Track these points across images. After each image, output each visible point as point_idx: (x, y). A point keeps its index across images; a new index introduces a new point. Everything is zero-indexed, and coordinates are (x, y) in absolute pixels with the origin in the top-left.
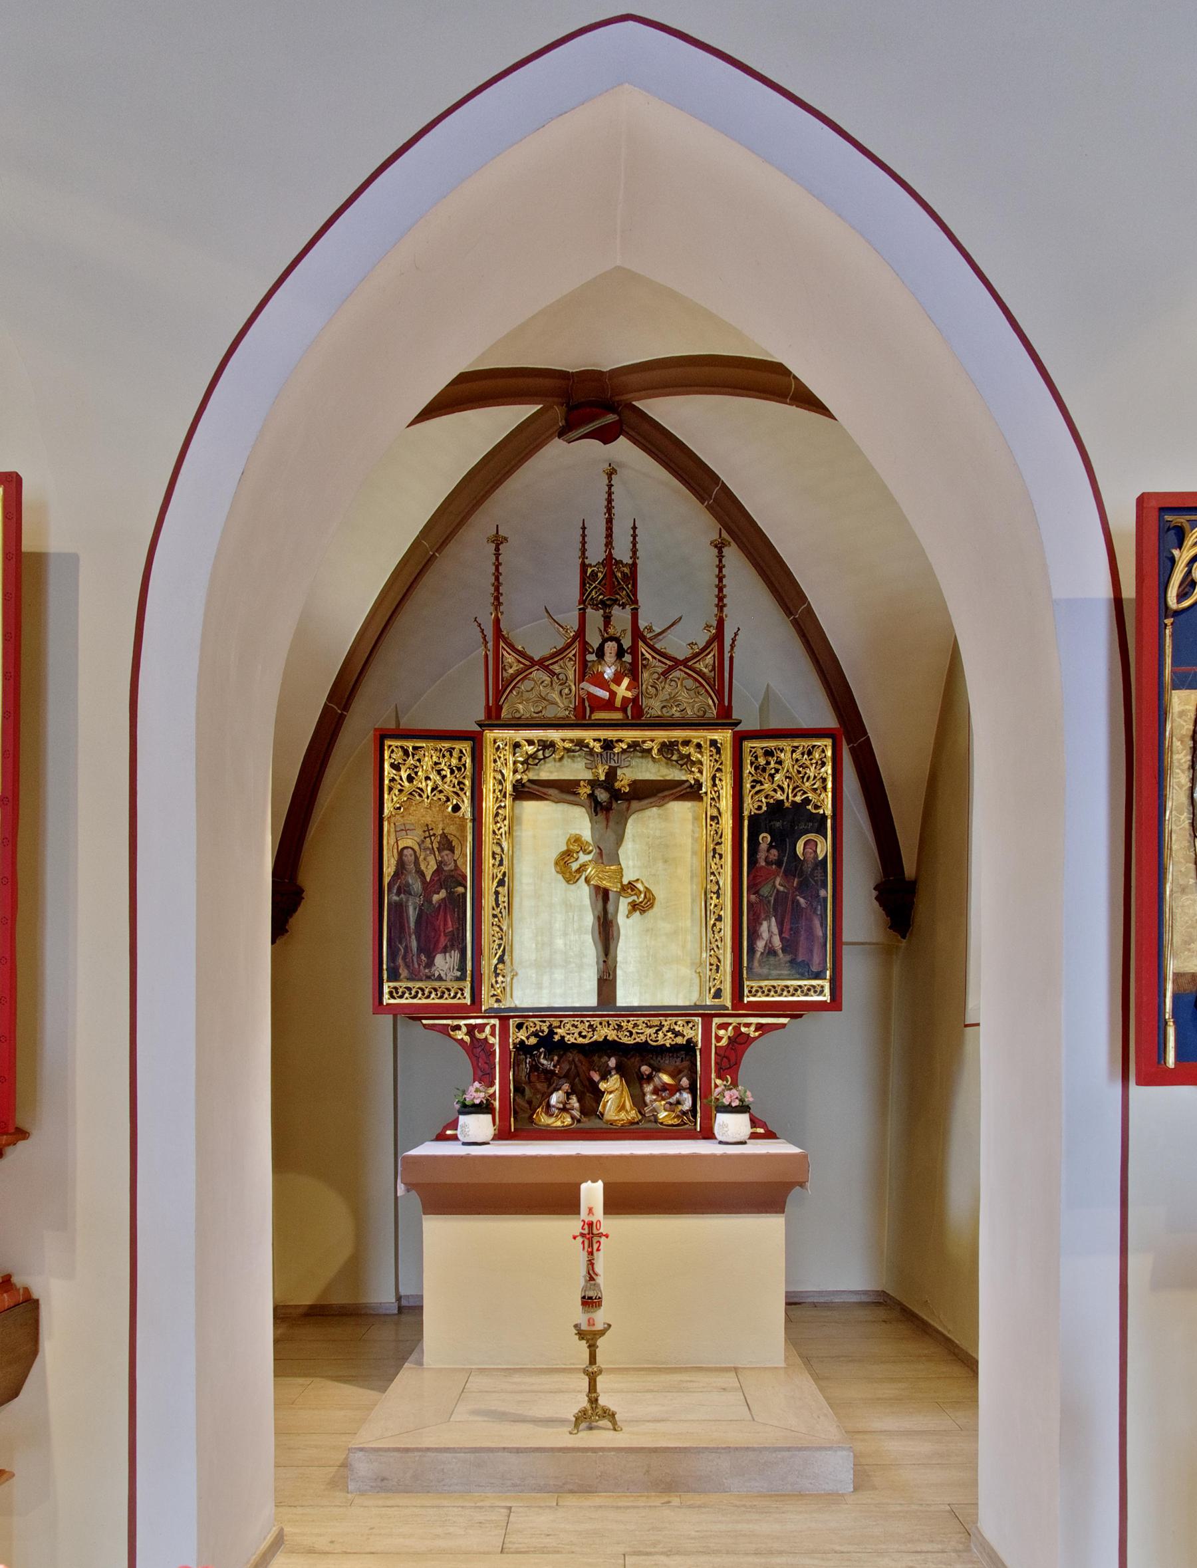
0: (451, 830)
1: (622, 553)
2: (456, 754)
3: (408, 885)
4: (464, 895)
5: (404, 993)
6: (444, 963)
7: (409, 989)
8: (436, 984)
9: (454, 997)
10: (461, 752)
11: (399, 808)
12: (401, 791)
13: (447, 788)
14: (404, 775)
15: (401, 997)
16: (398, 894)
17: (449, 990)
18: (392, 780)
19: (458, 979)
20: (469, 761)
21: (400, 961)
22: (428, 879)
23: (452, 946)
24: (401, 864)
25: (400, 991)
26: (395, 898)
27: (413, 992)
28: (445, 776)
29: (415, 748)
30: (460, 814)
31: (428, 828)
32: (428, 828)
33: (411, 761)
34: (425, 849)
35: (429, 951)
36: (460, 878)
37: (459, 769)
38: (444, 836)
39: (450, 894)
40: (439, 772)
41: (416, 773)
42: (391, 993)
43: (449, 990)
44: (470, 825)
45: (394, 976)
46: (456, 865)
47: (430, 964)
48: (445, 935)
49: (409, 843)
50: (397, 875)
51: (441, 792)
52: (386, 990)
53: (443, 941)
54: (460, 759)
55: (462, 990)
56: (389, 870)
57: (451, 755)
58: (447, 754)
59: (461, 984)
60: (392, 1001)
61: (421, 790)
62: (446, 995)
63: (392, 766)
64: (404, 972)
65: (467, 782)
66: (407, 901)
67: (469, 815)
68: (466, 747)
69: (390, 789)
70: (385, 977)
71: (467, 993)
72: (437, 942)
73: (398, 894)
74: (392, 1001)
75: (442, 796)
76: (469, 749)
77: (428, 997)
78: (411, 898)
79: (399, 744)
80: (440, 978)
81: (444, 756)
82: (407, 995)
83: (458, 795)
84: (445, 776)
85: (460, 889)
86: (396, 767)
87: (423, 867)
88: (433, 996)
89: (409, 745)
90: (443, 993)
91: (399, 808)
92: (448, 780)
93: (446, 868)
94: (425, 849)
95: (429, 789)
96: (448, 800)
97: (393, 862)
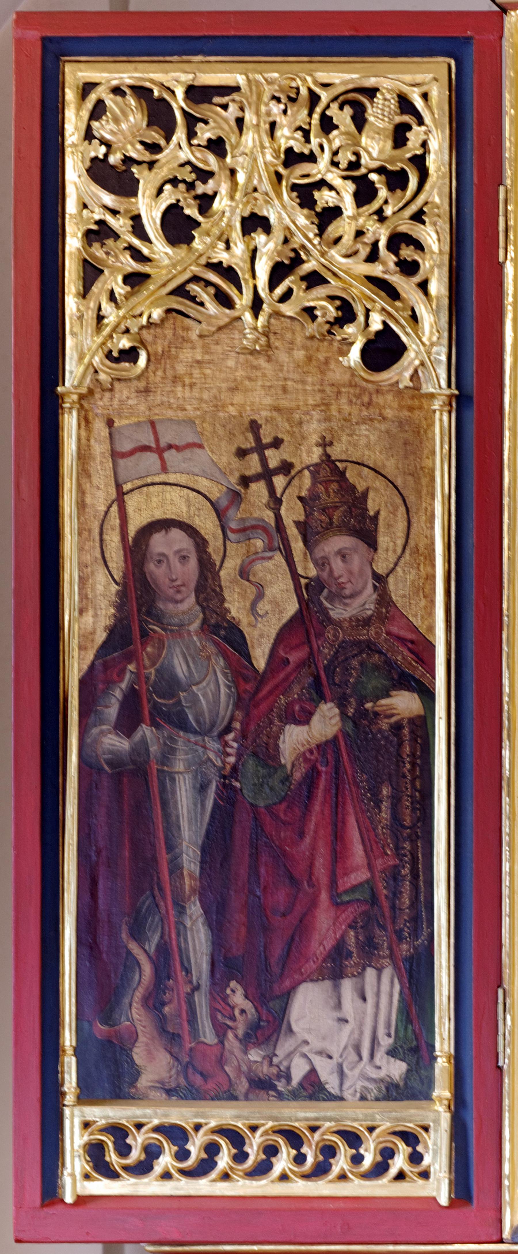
0: (364, 444)
1: (268, 408)
2: (382, 115)
3: (169, 685)
4: (422, 726)
5: (152, 1152)
6: (334, 1022)
7: (177, 1134)
8: (298, 1115)
9: (380, 1169)
10: (405, 104)
11: (130, 355)
12: (134, 280)
13: (347, 268)
14: (151, 212)
15: (142, 1169)
16: (127, 724)
17: (353, 1139)
18: (99, 233)
19: (393, 1092)
20: (438, 160)
21: (135, 1014)
22: (260, 661)
23: (369, 951)
24: (139, 597)
25: (137, 1142)
26: (114, 743)
27: (195, 1147)
28: (333, 213)
29: (198, 94)
30: (401, 373)
31: (256, 440)
32: (256, 440)
33: (179, 151)
34: (247, 530)
35: (263, 969)
36: (402, 656)
37: (396, 181)
38: (330, 470)
39: (360, 722)
40: (305, 195)
41: (206, 202)
42: (95, 1152)
43: (353, 1139)
44: (442, 423)
45: (110, 1076)
46: (384, 598)
47: (270, 1026)
48: (337, 904)
49: (173, 503)
50: (121, 642)
51: (314, 280)
52: (74, 1139)
53: (327, 927)
54: (399, 135)
55: (410, 1138)
56: (87, 618)
57: (360, 121)
58: (343, 118)
59: (409, 1115)
60: (102, 1187)
61: (229, 273)
62: (341, 1163)
63: (99, 171)
64: (152, 1062)
65: (434, 237)
66: (168, 753)
67: (438, 382)
68: (426, 80)
69: (91, 272)
70: (70, 1081)
71: (437, 1151)
72: (303, 928)
73: (127, 724)
74: (102, 1187)
75: (316, 298)
76: (439, 93)
77: (262, 1169)
78: (182, 739)
79: (127, 75)
80: (313, 1089)
81: (327, 125)
82: (166, 1161)
83: (392, 293)
84: (333, 213)
85: (405, 703)
86: (115, 177)
87: (236, 607)
88: (283, 1162)
89: (172, 79)
90: (329, 1151)
91: (130, 355)
92: (344, 227)
93: (338, 612)
94: (247, 530)
95: (263, 269)
96: (346, 313)
97: (106, 587)
